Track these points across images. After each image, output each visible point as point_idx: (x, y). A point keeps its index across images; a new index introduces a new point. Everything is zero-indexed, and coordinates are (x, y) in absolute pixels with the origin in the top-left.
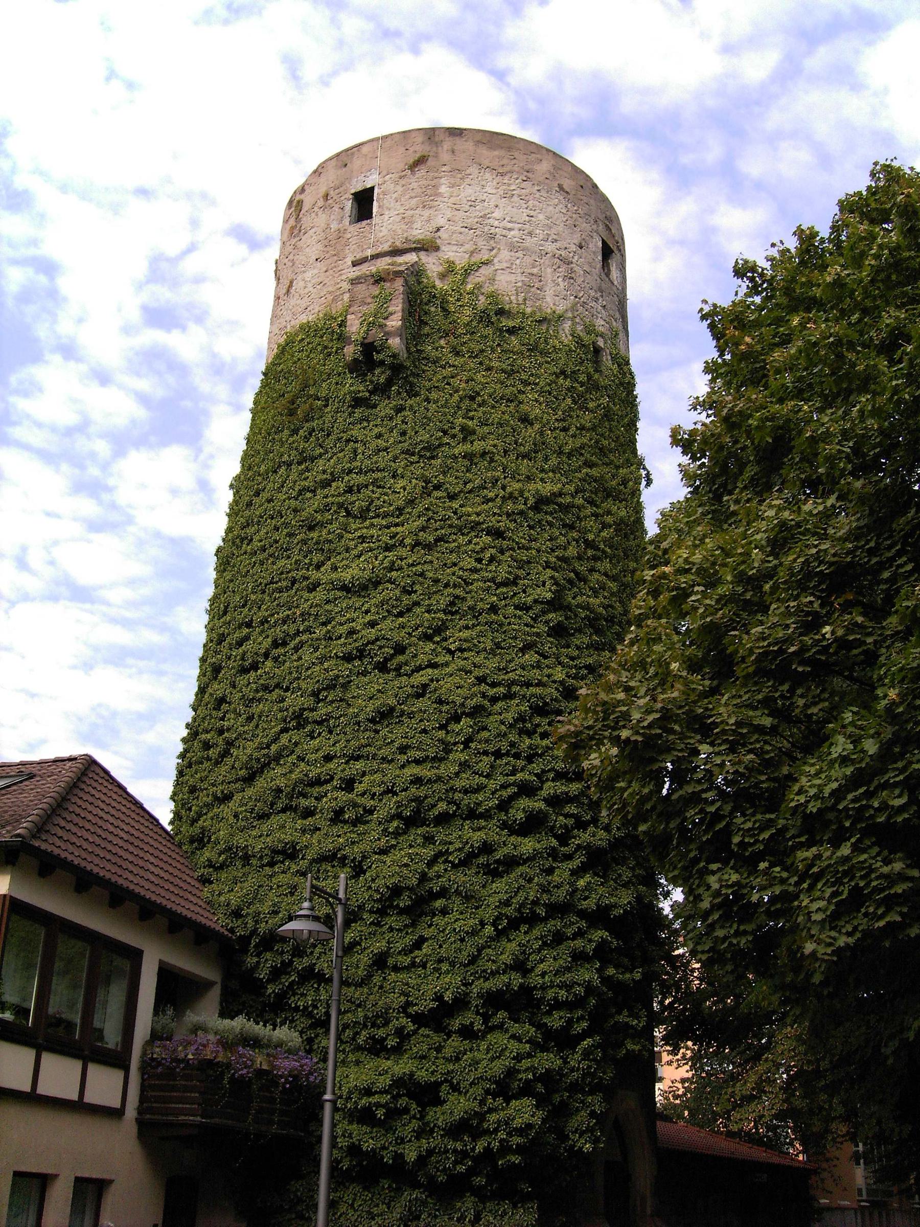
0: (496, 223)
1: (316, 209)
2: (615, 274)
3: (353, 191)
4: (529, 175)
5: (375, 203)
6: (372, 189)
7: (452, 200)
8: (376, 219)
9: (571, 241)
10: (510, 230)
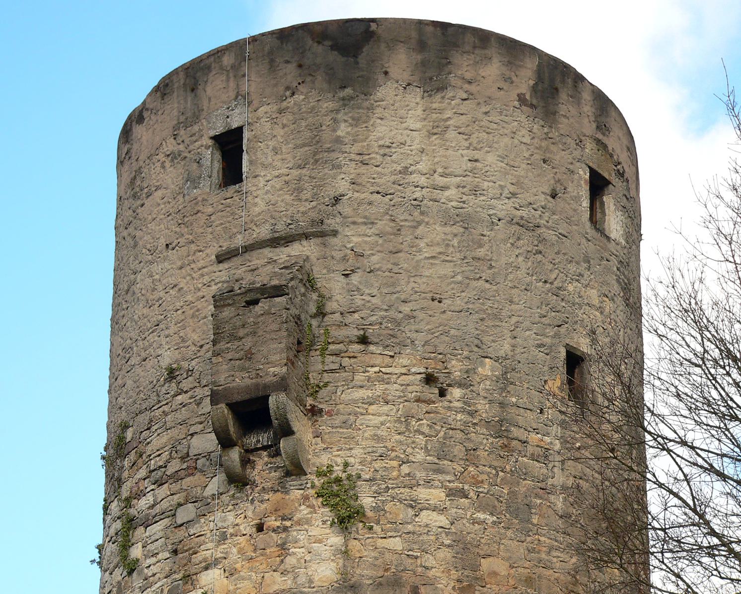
0: (423, 181)
1: (161, 157)
2: (614, 224)
3: (212, 133)
4: (473, 88)
5: (245, 157)
6: (240, 130)
7: (356, 148)
8: (247, 185)
9: (537, 192)
10: (444, 188)
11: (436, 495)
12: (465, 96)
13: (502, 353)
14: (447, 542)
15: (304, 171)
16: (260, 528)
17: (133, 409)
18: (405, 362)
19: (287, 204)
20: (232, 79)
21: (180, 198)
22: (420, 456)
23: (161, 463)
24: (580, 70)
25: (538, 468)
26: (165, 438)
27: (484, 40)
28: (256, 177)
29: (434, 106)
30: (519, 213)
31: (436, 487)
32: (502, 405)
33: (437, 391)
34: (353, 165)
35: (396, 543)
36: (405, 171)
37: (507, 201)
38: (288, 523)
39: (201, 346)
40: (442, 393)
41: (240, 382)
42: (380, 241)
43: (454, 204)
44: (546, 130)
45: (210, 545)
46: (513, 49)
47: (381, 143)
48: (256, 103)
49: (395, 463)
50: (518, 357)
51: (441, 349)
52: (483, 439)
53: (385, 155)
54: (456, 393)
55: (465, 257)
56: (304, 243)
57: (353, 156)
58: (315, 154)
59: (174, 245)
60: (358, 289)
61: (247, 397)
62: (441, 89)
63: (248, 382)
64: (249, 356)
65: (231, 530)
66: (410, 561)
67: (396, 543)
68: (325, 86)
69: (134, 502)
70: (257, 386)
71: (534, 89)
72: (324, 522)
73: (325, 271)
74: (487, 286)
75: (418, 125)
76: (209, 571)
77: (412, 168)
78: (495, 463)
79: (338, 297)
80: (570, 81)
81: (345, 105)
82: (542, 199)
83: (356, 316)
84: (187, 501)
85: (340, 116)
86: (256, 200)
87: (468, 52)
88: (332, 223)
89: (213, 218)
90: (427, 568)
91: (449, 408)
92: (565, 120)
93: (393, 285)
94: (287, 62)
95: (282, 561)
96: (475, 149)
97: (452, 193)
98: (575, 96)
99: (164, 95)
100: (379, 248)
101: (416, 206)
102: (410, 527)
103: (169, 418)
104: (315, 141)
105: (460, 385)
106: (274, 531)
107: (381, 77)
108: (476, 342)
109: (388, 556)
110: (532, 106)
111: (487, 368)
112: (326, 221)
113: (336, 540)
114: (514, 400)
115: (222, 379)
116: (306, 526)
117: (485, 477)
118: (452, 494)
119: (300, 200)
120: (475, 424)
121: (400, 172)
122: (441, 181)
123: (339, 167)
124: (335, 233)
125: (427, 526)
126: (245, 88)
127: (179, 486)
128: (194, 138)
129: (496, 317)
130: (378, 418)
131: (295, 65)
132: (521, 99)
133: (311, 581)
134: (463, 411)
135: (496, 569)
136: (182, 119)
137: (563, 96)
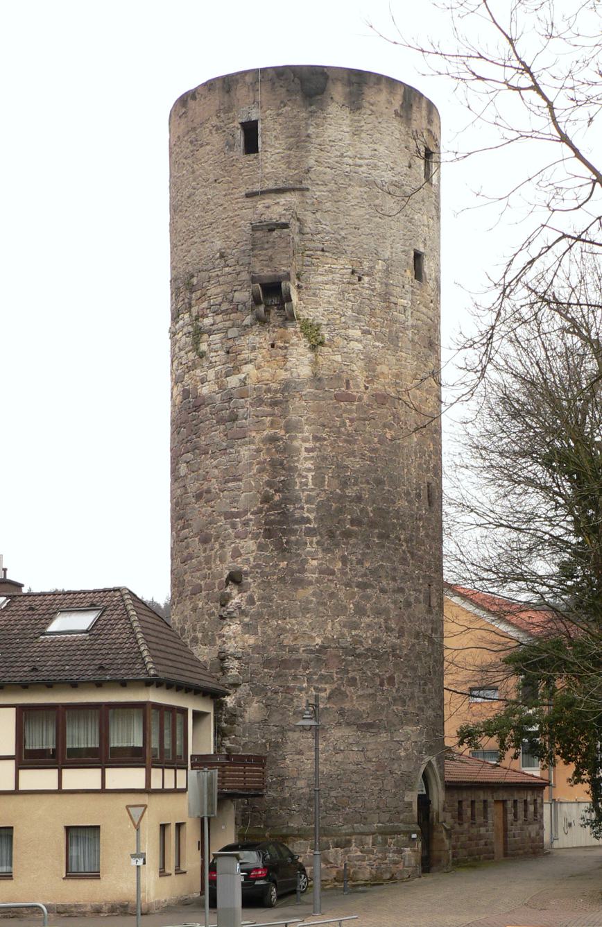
0: (350, 162)
3: (240, 121)
5: (260, 139)
6: (256, 122)
8: (261, 155)
10: (360, 166)
11: (356, 333)
12: (370, 113)
13: (386, 257)
14: (362, 357)
15: (291, 152)
16: (273, 346)
17: (196, 267)
18: (343, 262)
19: (283, 170)
20: (251, 91)
21: (222, 154)
22: (349, 313)
23: (217, 303)
24: (421, 92)
25: (402, 317)
26: (219, 290)
27: (379, 78)
28: (265, 151)
29: (356, 118)
30: (395, 179)
31: (357, 329)
32: (387, 285)
33: (357, 278)
34: (316, 150)
35: (338, 358)
36: (342, 156)
37: (389, 172)
38: (287, 345)
39: (238, 243)
40: (360, 279)
41: (267, 273)
42: (330, 195)
43: (365, 175)
44: (407, 129)
45: (247, 351)
46: (392, 83)
47: (330, 139)
48: (264, 108)
49: (338, 316)
50: (394, 258)
51: (359, 255)
52: (378, 303)
53: (332, 146)
54: (366, 279)
55: (370, 205)
56: (293, 193)
57: (316, 146)
58: (297, 142)
59: (220, 180)
60: (320, 222)
61: (270, 281)
62: (359, 108)
63: (271, 273)
64: (271, 259)
65: (258, 345)
66: (346, 367)
67: (338, 358)
68: (302, 103)
69: (201, 319)
70: (275, 276)
71: (402, 106)
72: (305, 346)
73: (303, 210)
74: (380, 220)
75: (348, 130)
76: (247, 365)
77: (345, 154)
78: (384, 316)
79: (310, 225)
80: (417, 99)
81: (312, 116)
82: (405, 170)
83: (319, 236)
84: (233, 326)
85: (309, 122)
86: (267, 165)
87: (372, 87)
88: (306, 184)
89: (242, 171)
90: (353, 371)
91: (363, 288)
92: (415, 122)
93: (337, 220)
94: (281, 86)
95: (285, 364)
96: (375, 143)
97: (364, 168)
98: (420, 102)
99: (209, 90)
100: (330, 199)
101: (347, 176)
102: (345, 350)
103: (221, 279)
104: (297, 135)
105: (368, 275)
106: (280, 348)
107: (330, 102)
108: (375, 251)
109: (335, 364)
110: (401, 116)
111: (380, 266)
112: (303, 182)
113: (310, 355)
114: (391, 282)
115: (257, 270)
116: (296, 347)
117: (378, 323)
118: (365, 332)
119: (289, 168)
120: (374, 296)
121: (340, 156)
122: (359, 162)
123: (309, 151)
124: (308, 189)
125: (353, 349)
126: (259, 98)
127: (228, 318)
128: (230, 121)
129: (384, 237)
130: (330, 292)
131: (285, 89)
132: (396, 112)
133: (299, 376)
134: (369, 289)
135: (383, 370)
136: (222, 107)
137: (414, 108)
